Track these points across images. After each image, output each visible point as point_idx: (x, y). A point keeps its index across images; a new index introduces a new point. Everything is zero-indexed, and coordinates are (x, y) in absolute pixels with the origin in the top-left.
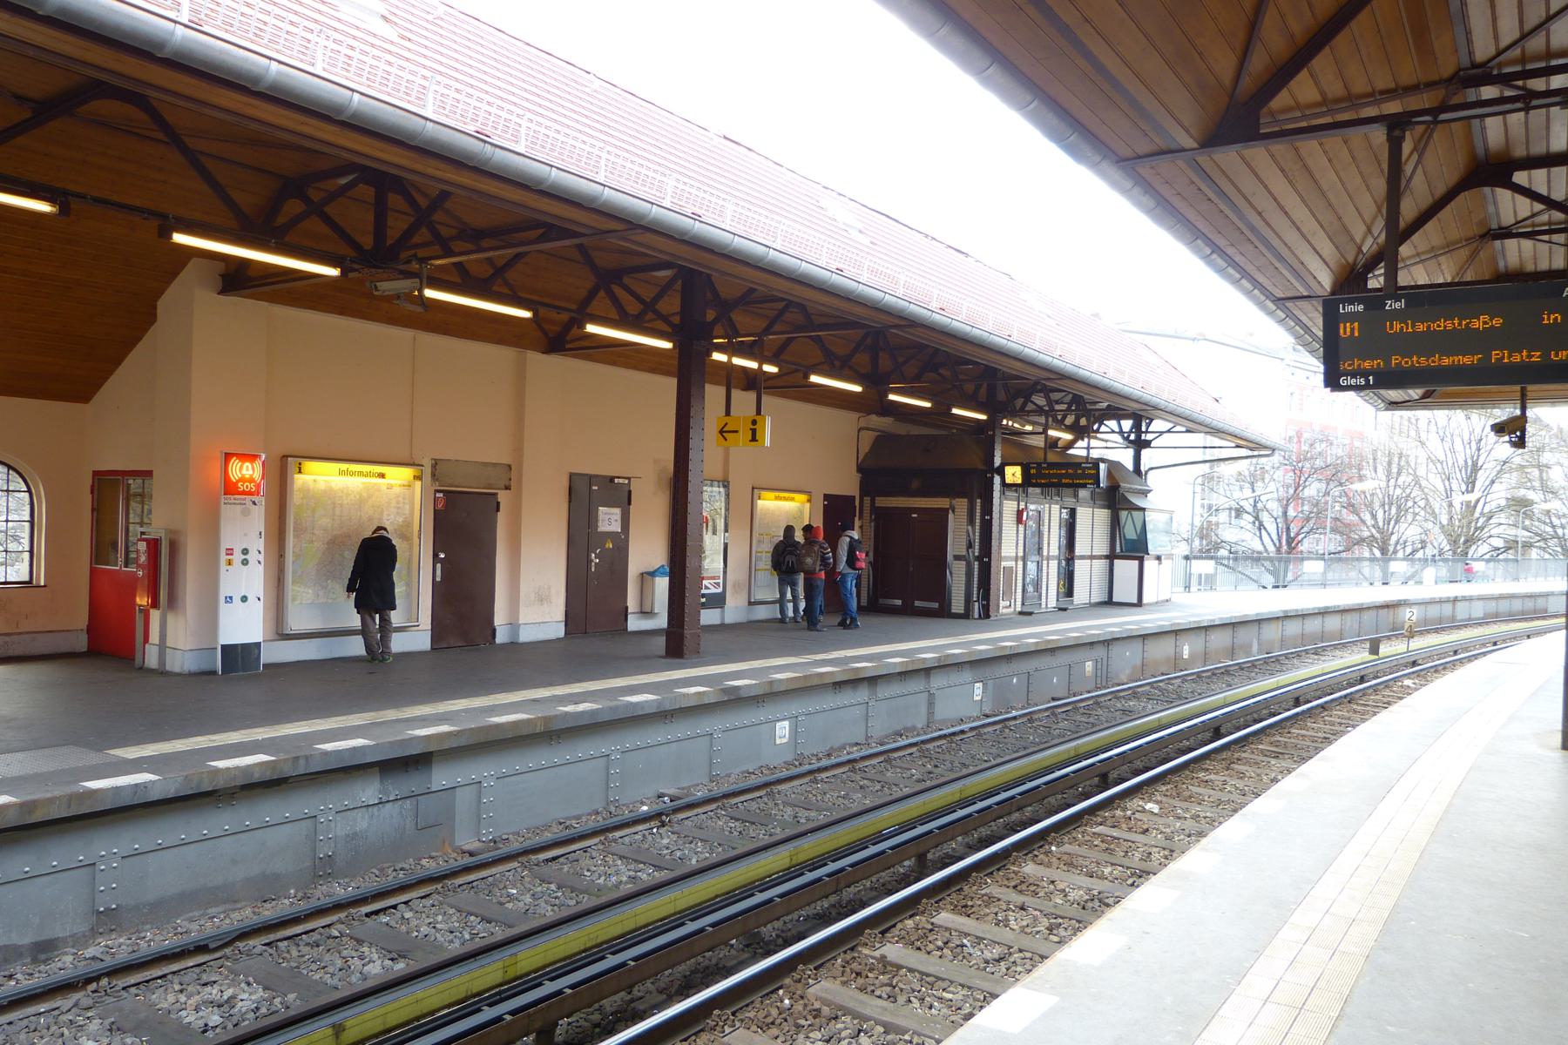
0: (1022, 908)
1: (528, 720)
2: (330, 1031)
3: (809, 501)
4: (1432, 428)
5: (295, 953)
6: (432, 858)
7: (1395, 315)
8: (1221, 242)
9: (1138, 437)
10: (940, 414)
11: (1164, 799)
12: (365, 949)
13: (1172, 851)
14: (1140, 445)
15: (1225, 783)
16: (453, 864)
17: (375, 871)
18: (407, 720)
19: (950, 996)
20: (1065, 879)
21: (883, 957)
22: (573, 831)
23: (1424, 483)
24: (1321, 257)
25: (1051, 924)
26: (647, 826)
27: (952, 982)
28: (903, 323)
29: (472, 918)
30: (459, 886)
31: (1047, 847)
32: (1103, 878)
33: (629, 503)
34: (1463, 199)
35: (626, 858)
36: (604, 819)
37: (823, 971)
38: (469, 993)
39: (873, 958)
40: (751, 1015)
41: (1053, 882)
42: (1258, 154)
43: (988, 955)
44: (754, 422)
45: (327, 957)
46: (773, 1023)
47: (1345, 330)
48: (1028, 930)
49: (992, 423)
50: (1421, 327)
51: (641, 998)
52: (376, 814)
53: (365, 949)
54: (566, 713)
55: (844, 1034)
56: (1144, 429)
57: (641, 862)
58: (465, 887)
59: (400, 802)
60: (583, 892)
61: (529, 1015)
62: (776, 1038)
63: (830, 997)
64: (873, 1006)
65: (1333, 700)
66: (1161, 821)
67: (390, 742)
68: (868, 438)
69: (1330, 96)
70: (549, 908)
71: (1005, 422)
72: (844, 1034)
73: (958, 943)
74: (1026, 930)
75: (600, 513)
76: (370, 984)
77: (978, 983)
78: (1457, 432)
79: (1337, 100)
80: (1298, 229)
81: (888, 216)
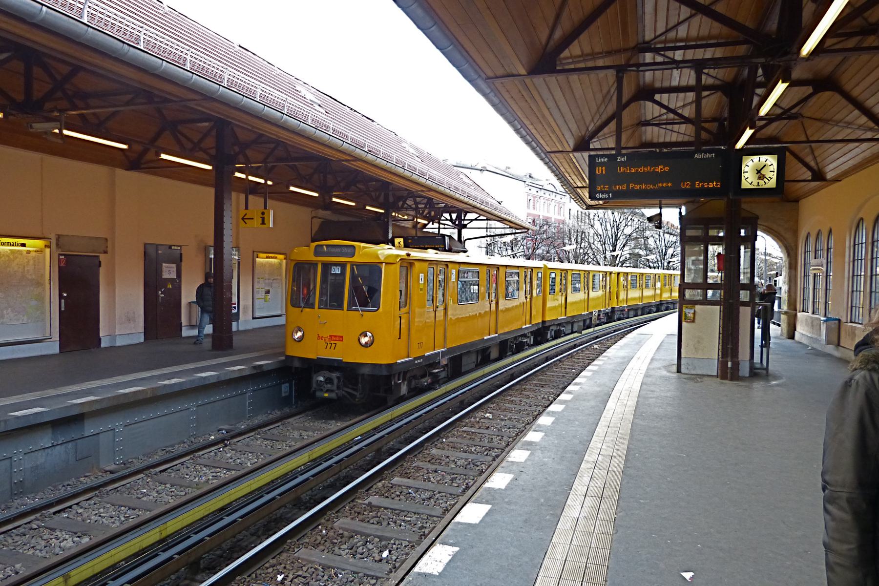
0: (436, 471)
1: (143, 390)
2: (61, 579)
3: (285, 259)
4: (596, 218)
5: (10, 541)
6: (87, 477)
7: (622, 164)
8: (527, 122)
9: (460, 222)
10: (360, 208)
11: (493, 411)
12: (58, 533)
13: (502, 437)
14: (461, 227)
15: (521, 401)
16: (102, 480)
17: (50, 487)
18: (64, 395)
19: (409, 519)
20: (454, 455)
21: (370, 503)
22: (172, 454)
23: (593, 246)
24: (571, 132)
25: (452, 478)
26: (216, 447)
27: (408, 512)
28: (349, 158)
29: (123, 508)
30: (110, 490)
31: (441, 440)
32: (471, 453)
33: (181, 261)
34: (633, 105)
35: (208, 466)
36: (189, 446)
37: (340, 514)
38: (141, 548)
39: (364, 504)
40: (307, 540)
41: (448, 457)
42: (552, 79)
43: (423, 496)
44: (263, 213)
45: (33, 541)
46: (320, 543)
47: (599, 170)
48: (441, 482)
49: (387, 214)
50: (633, 170)
51: (242, 539)
52: (50, 453)
53: (58, 533)
54: (165, 385)
55: (358, 545)
56: (463, 218)
57: (218, 468)
58: (113, 491)
59: (65, 445)
60: (187, 487)
61: (188, 554)
62: (323, 550)
63: (347, 526)
64: (371, 529)
65: (564, 357)
66: (494, 422)
67: (58, 408)
68: (317, 223)
69: (585, 52)
70: (170, 498)
71: (394, 214)
72: (358, 545)
73: (407, 492)
74: (440, 482)
75: (163, 267)
76: (67, 554)
77: (421, 511)
78: (608, 221)
79: (587, 55)
80: (563, 117)
81: (331, 97)
